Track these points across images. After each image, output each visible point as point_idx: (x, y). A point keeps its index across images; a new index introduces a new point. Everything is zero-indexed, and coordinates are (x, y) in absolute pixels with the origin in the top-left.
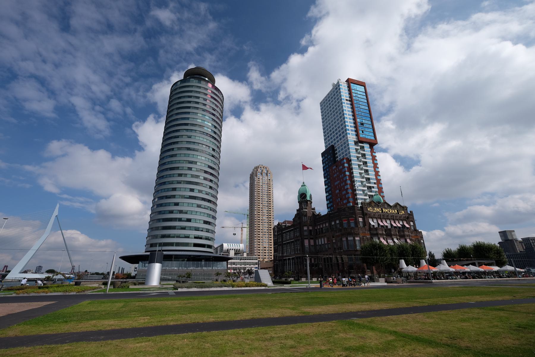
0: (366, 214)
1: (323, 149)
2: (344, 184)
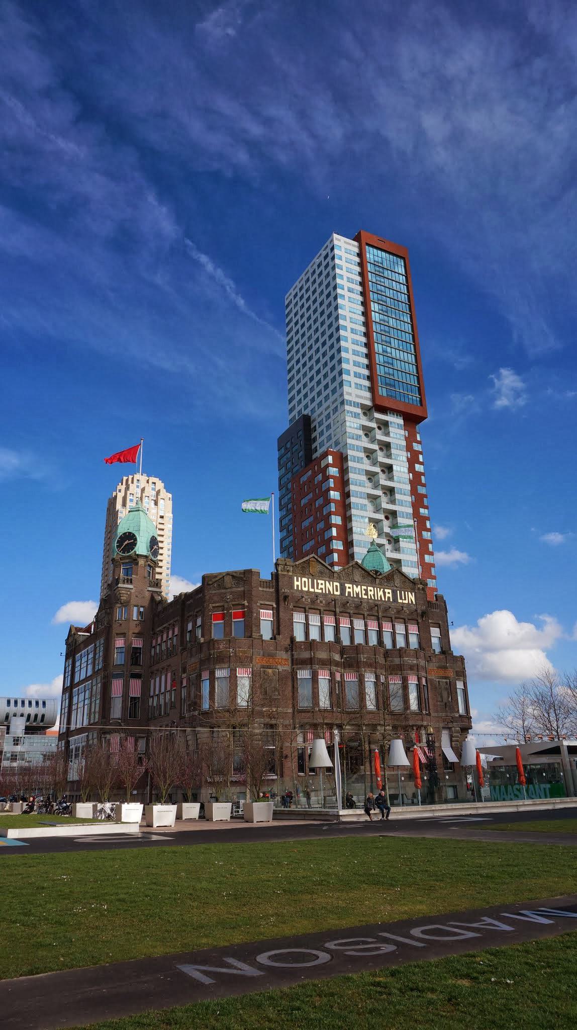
0: (286, 598)
1: (284, 426)
2: (320, 477)
